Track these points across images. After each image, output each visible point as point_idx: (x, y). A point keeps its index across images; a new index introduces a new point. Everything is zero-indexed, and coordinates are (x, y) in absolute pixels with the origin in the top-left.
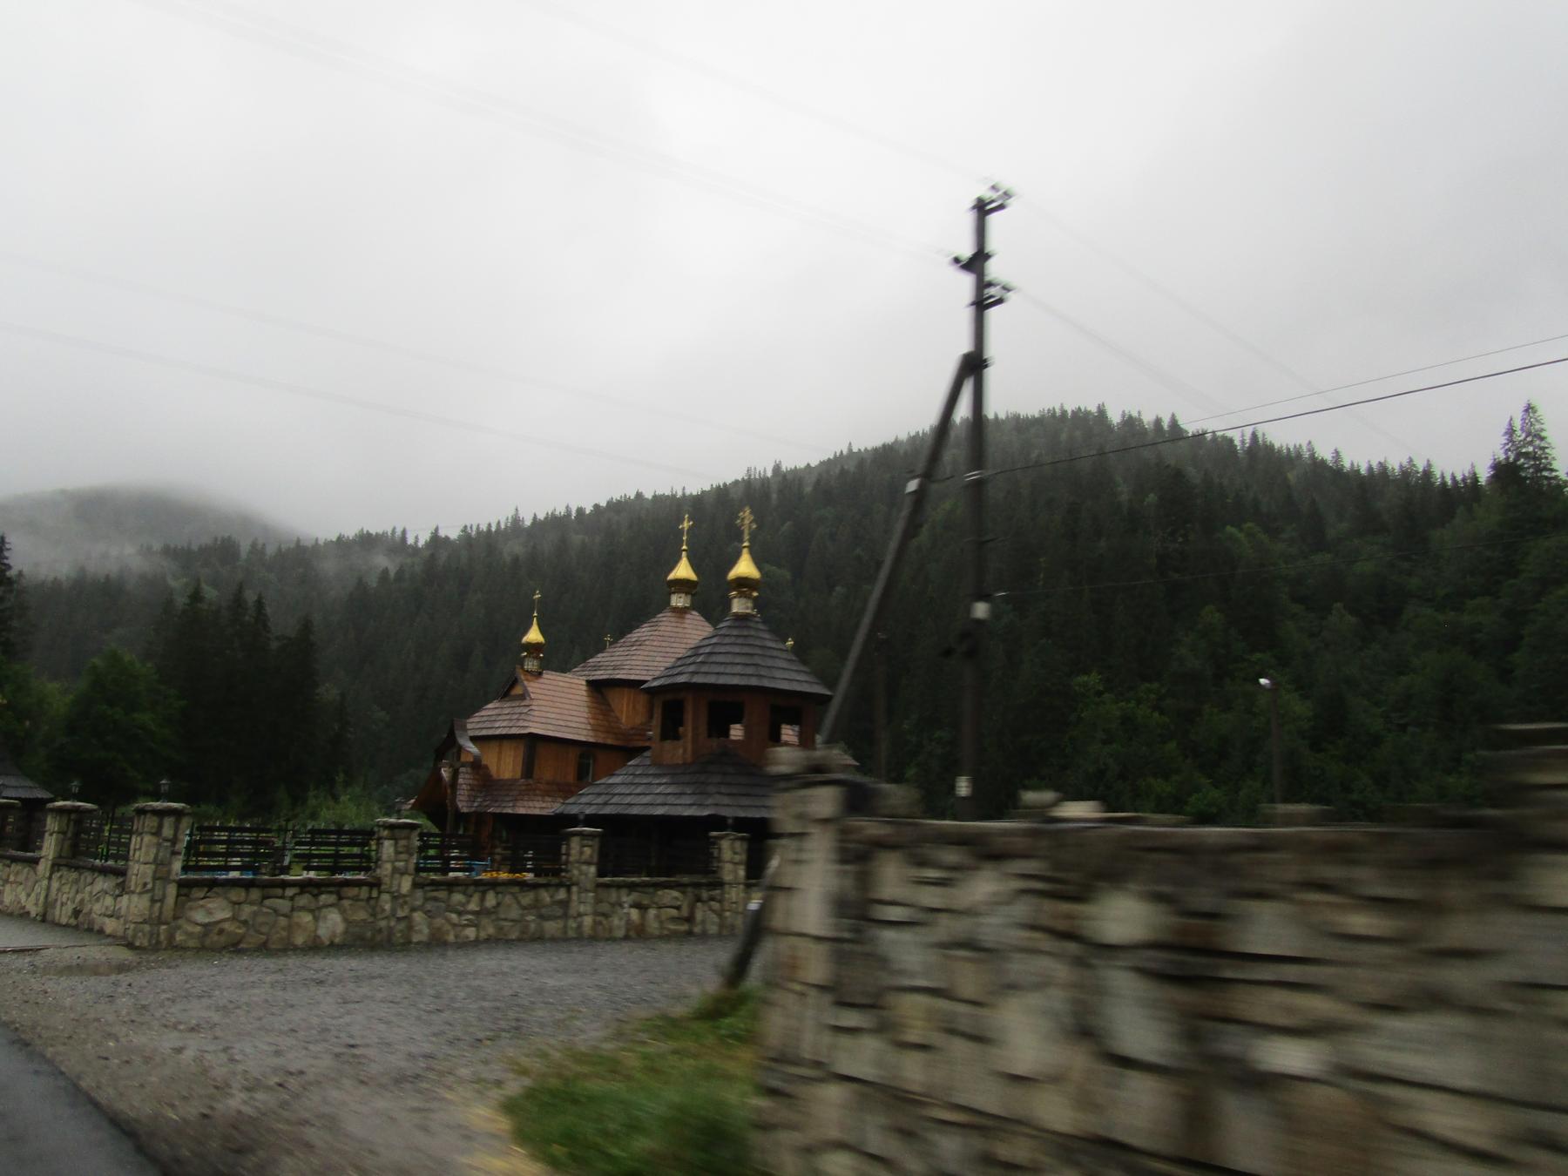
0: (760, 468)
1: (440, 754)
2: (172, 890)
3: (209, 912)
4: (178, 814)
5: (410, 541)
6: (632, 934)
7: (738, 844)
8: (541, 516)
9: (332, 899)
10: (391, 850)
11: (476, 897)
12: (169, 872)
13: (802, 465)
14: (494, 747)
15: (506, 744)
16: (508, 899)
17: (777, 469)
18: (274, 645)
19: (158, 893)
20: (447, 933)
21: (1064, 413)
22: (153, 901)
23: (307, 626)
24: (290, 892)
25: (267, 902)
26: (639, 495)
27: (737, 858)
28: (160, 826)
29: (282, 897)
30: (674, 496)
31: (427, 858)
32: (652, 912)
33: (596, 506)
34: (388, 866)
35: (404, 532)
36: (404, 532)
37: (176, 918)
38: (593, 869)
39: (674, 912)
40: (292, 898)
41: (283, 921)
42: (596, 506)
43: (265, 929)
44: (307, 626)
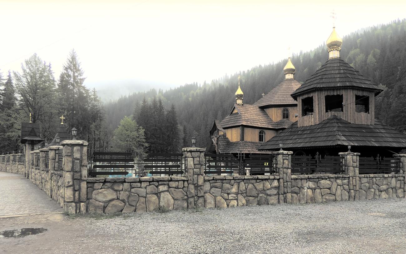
0: (296, 53)
1: (212, 133)
2: (84, 185)
3: (105, 196)
4: (82, 145)
5: (199, 86)
6: (309, 201)
7: (355, 157)
8: (233, 75)
9: (165, 188)
10: (192, 163)
11: (236, 186)
12: (81, 176)
13: (309, 51)
14: (229, 130)
15: (233, 129)
16: (250, 186)
17: (301, 53)
18: (166, 113)
19: (77, 187)
20: (223, 203)
21: (399, 21)
22: (75, 191)
23: (173, 108)
24: (144, 185)
25: (133, 190)
26: (260, 66)
27: (355, 164)
28: (72, 152)
29: (141, 187)
30: (270, 65)
31: (210, 167)
32: (318, 191)
33: (248, 70)
34: (191, 171)
35: (197, 83)
36: (197, 83)
37: (88, 199)
38: (289, 171)
39: (328, 191)
40: (146, 188)
41: (142, 200)
42: (248, 70)
43: (134, 204)
44: (173, 108)
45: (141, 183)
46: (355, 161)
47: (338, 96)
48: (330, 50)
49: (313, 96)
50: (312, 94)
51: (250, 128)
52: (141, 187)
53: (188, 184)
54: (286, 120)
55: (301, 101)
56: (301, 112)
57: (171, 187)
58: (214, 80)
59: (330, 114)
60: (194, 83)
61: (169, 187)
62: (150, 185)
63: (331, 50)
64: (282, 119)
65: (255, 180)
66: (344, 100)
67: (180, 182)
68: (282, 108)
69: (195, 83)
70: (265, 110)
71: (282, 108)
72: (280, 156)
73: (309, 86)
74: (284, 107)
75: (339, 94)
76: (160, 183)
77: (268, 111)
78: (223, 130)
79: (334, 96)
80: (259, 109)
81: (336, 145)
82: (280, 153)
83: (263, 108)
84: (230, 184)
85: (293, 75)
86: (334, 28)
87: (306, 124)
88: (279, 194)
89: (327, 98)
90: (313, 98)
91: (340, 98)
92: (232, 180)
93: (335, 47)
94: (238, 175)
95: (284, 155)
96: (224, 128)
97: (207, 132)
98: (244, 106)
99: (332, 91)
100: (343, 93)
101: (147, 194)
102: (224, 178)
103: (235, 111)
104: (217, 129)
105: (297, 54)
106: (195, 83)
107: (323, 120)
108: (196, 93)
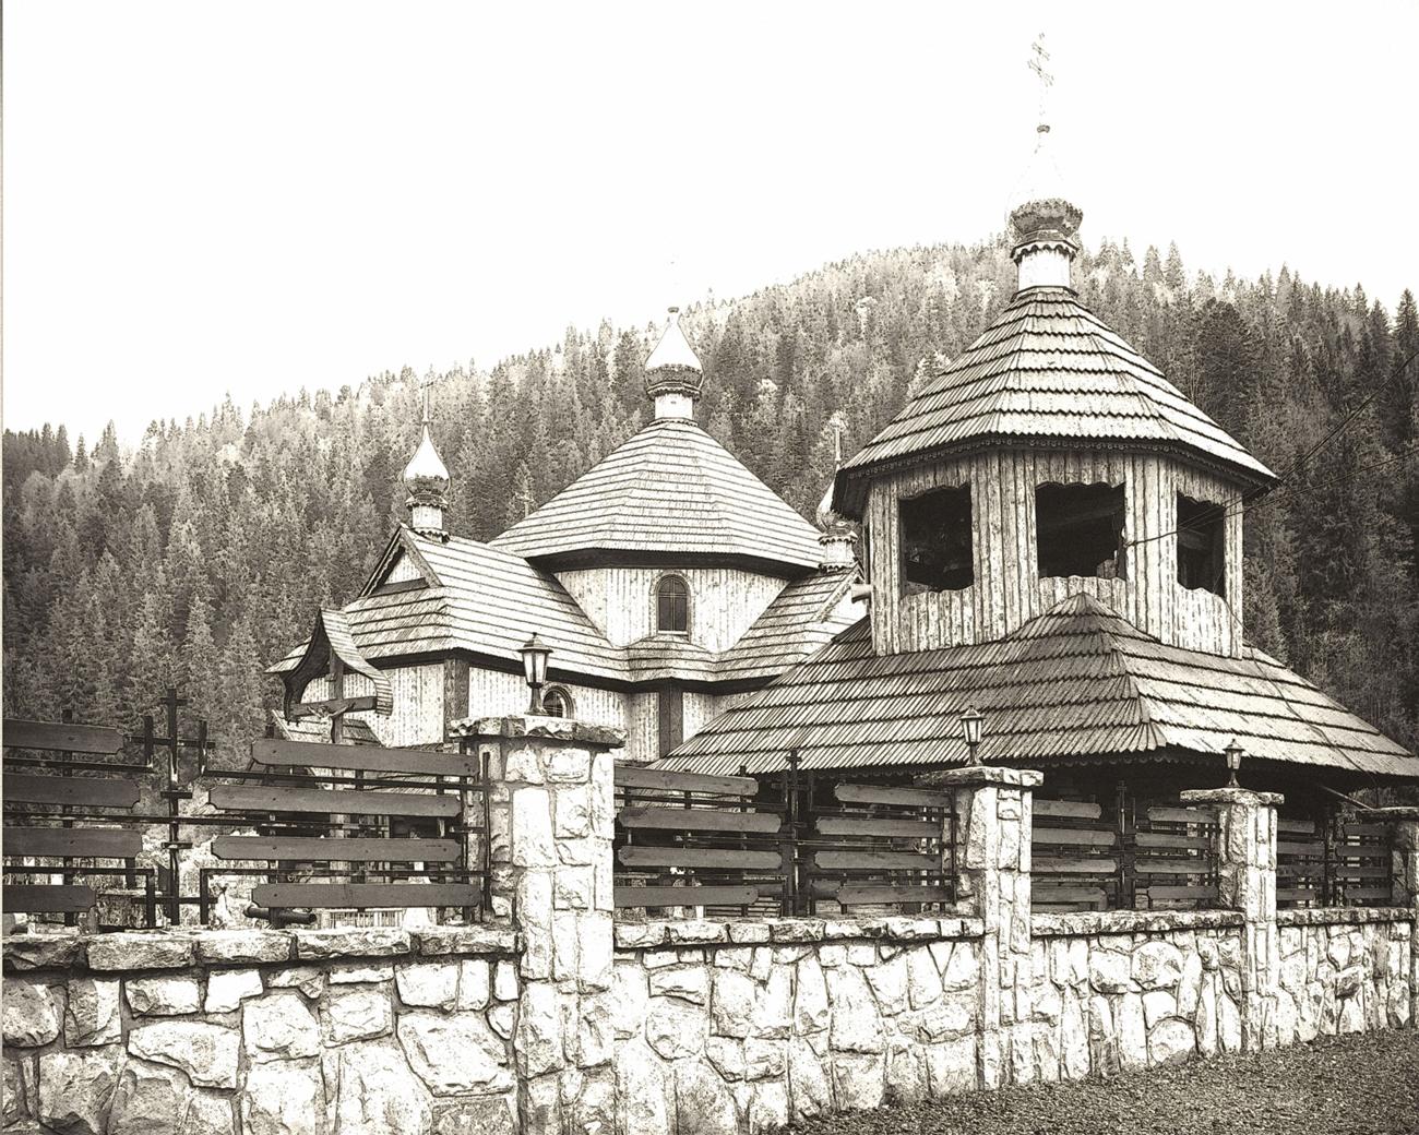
35: (61, 430)
45: (203, 981)
46: (1266, 836)
47: (1099, 488)
48: (1029, 247)
49: (974, 486)
50: (963, 472)
51: (497, 669)
52: (207, 1014)
53: (524, 982)
54: (677, 639)
55: (894, 510)
56: (895, 568)
57: (411, 1008)
58: (163, 424)
59: (1060, 590)
60: (46, 427)
61: (401, 1008)
62: (268, 990)
63: (1035, 249)
64: (653, 632)
65: (116, 985)
66: (1129, 520)
67: (469, 965)
68: (656, 572)
69: (54, 430)
70: (559, 577)
71: (652, 575)
72: (987, 796)
73: (946, 424)
74: (665, 569)
75: (1104, 480)
76: (340, 976)
77: (575, 582)
78: (371, 670)
79: (1079, 487)
80: (530, 572)
81: (1136, 750)
82: (988, 777)
83: (548, 568)
84: (749, 976)
85: (689, 401)
86: (1044, 129)
87: (927, 637)
88: (979, 1031)
89: (1049, 499)
90: (973, 494)
91: (1113, 498)
92: (760, 950)
93: (1055, 236)
94: (302, 940)
95: (1005, 794)
96: (381, 663)
97: (125, 707)
98: (449, 544)
99: (1070, 460)
100: (1126, 474)
101: (244, 1062)
102: (724, 932)
103: (404, 572)
104: (332, 663)
105: (588, 332)
106: (54, 430)
107: (1026, 617)
108: (58, 487)
